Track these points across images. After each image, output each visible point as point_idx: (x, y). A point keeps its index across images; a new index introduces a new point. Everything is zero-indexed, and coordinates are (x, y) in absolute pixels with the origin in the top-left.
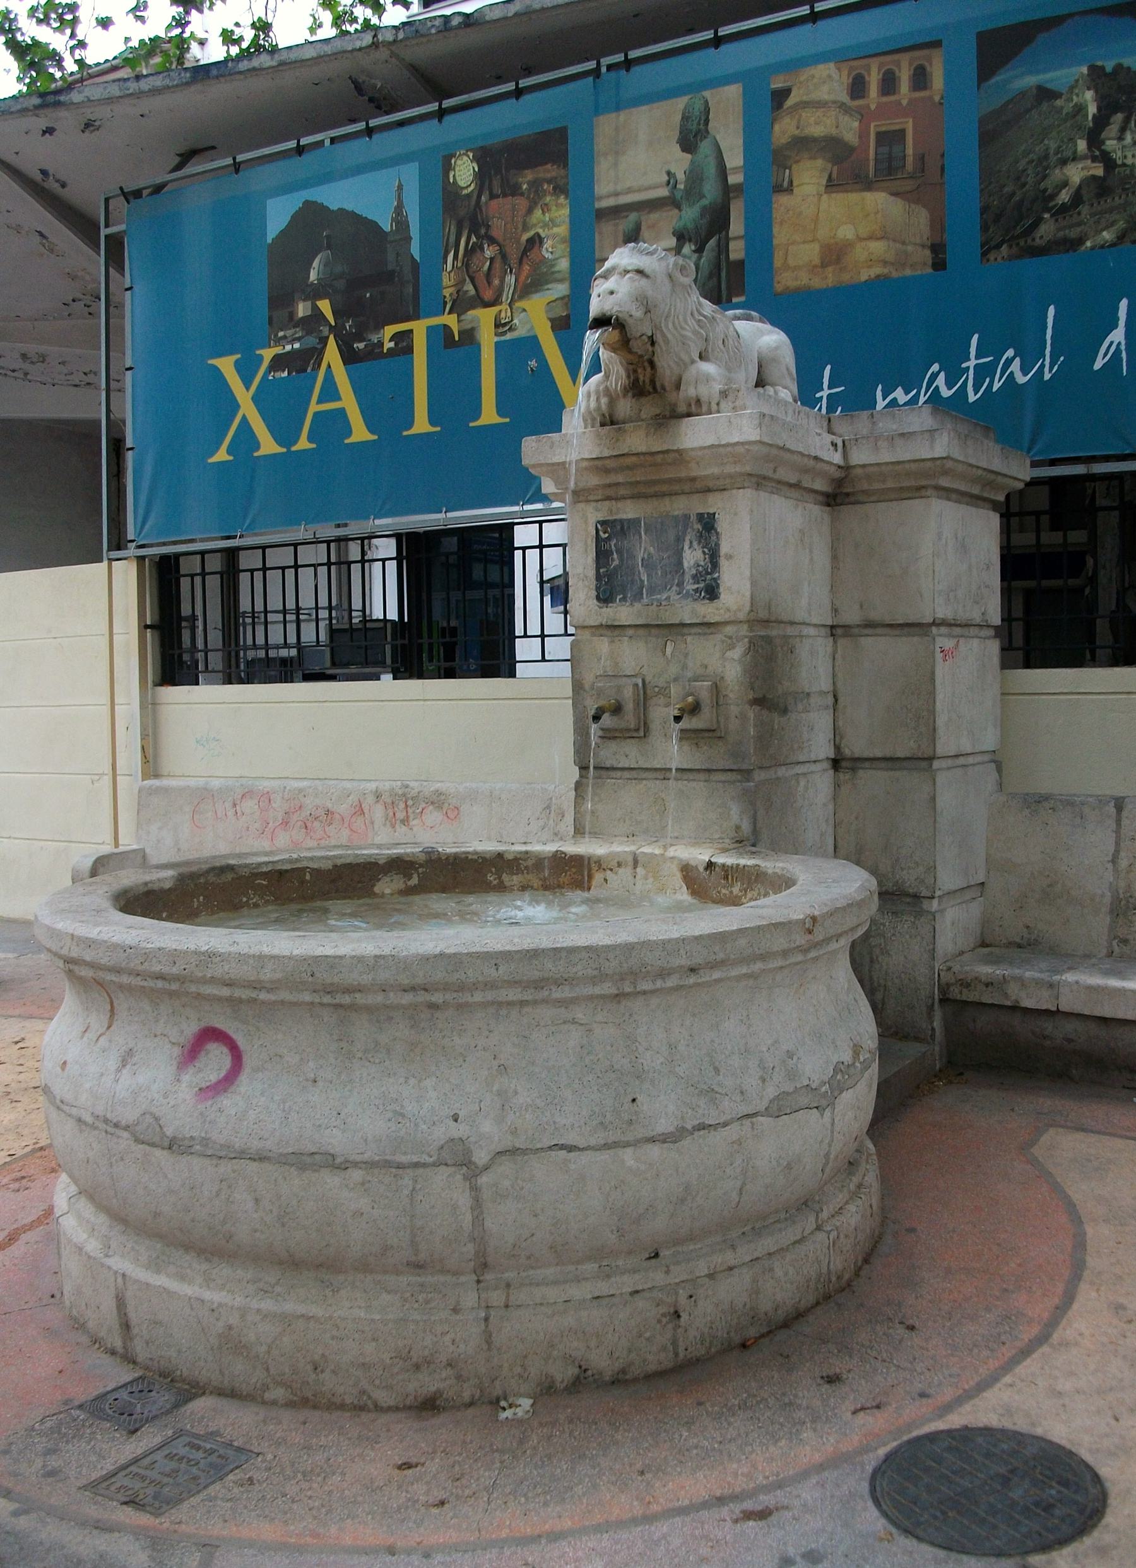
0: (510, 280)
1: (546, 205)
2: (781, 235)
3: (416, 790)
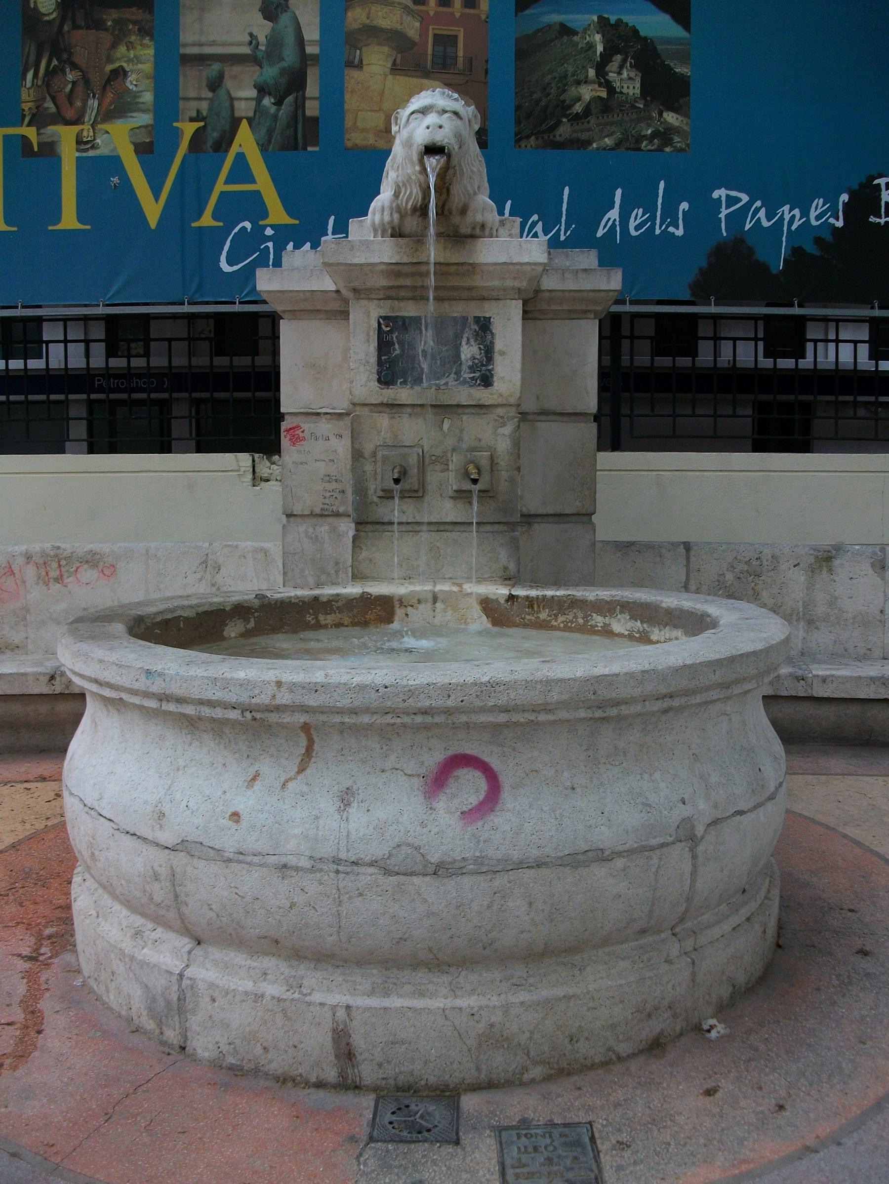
0: (93, 103)
1: (131, 43)
2: (351, 102)
3: (70, 551)
